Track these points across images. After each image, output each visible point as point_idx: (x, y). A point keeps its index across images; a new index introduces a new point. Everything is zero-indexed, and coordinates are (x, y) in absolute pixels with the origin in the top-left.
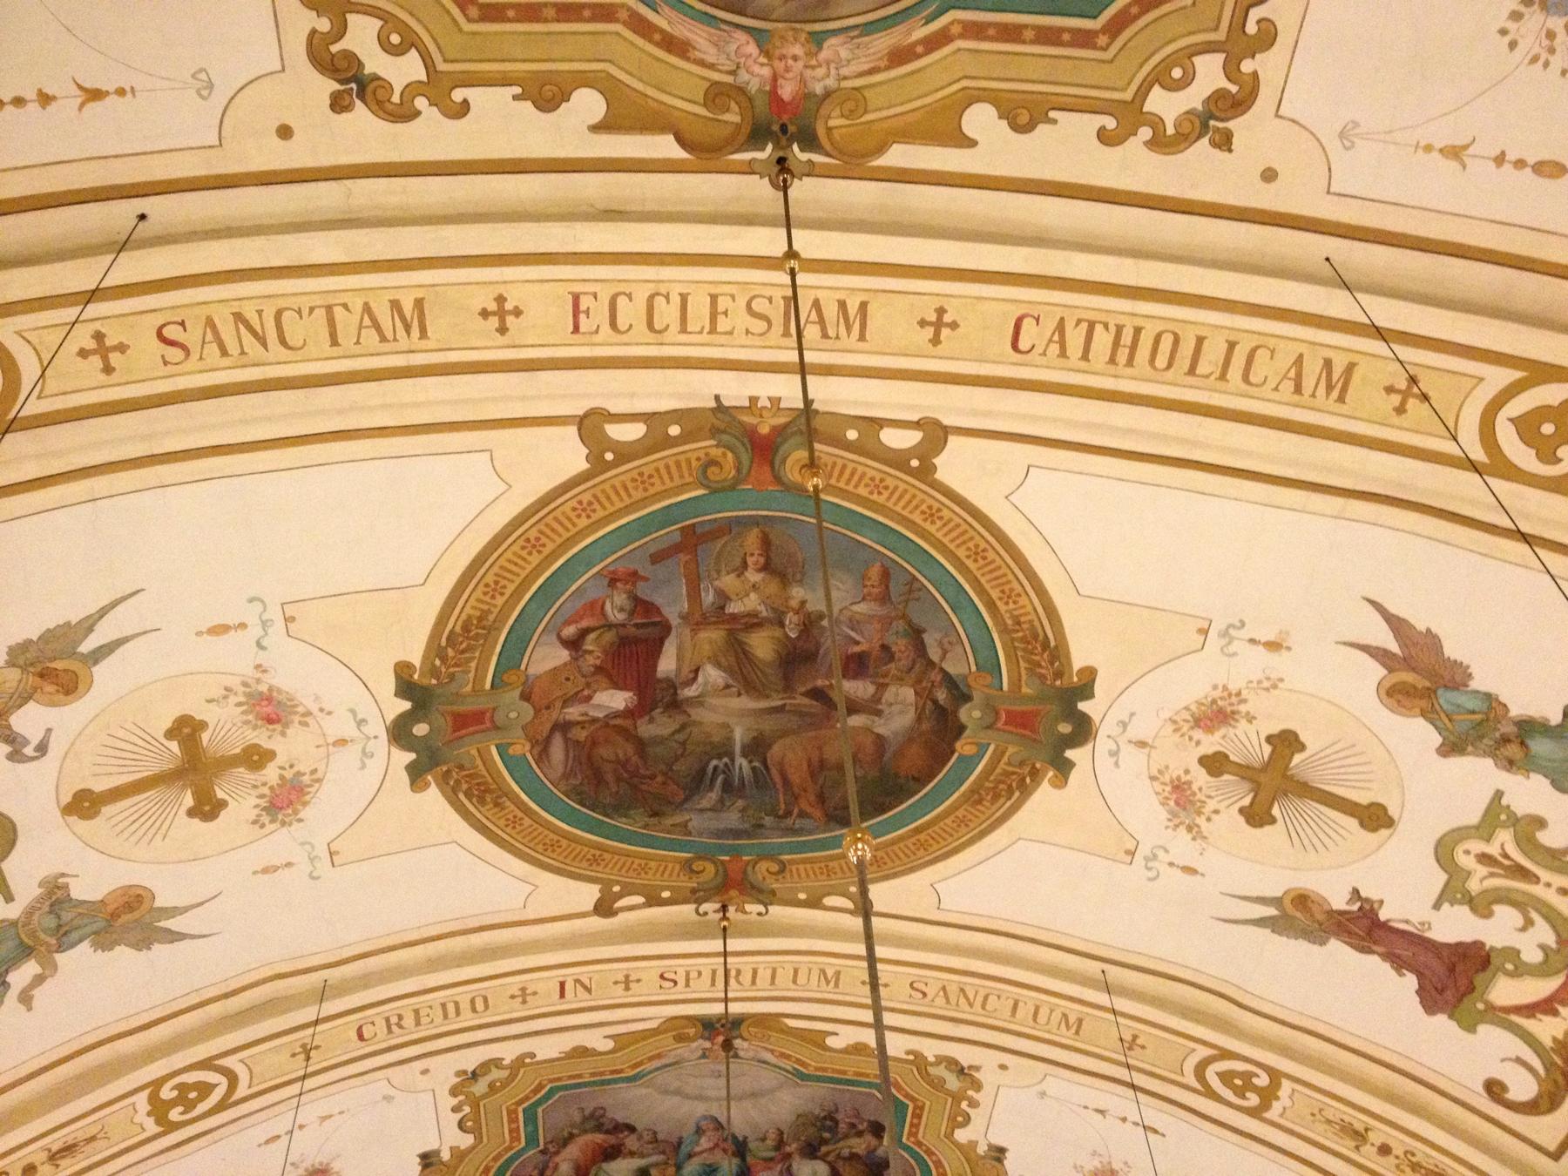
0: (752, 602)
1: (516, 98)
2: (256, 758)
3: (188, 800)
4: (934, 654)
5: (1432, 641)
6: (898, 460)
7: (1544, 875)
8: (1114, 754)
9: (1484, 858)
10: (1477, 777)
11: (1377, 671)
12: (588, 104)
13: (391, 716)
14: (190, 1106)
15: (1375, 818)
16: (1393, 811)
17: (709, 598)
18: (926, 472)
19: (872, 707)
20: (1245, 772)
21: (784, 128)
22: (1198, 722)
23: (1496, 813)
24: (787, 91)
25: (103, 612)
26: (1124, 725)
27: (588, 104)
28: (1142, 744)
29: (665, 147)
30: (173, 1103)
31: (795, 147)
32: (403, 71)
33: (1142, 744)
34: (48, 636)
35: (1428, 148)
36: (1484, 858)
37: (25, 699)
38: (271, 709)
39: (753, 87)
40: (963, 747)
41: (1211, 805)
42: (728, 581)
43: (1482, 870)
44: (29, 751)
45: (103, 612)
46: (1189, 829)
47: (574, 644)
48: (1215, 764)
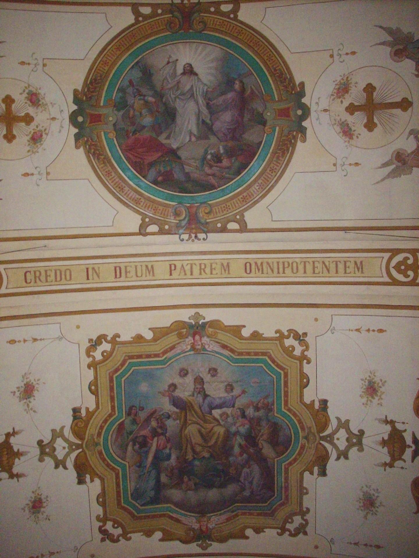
1: (263, 334)
6: (153, 222)
21: (197, 328)
24: (204, 529)
27: (158, 535)
31: (194, 323)
32: (289, 342)
35: (41, 340)
39: (196, 528)
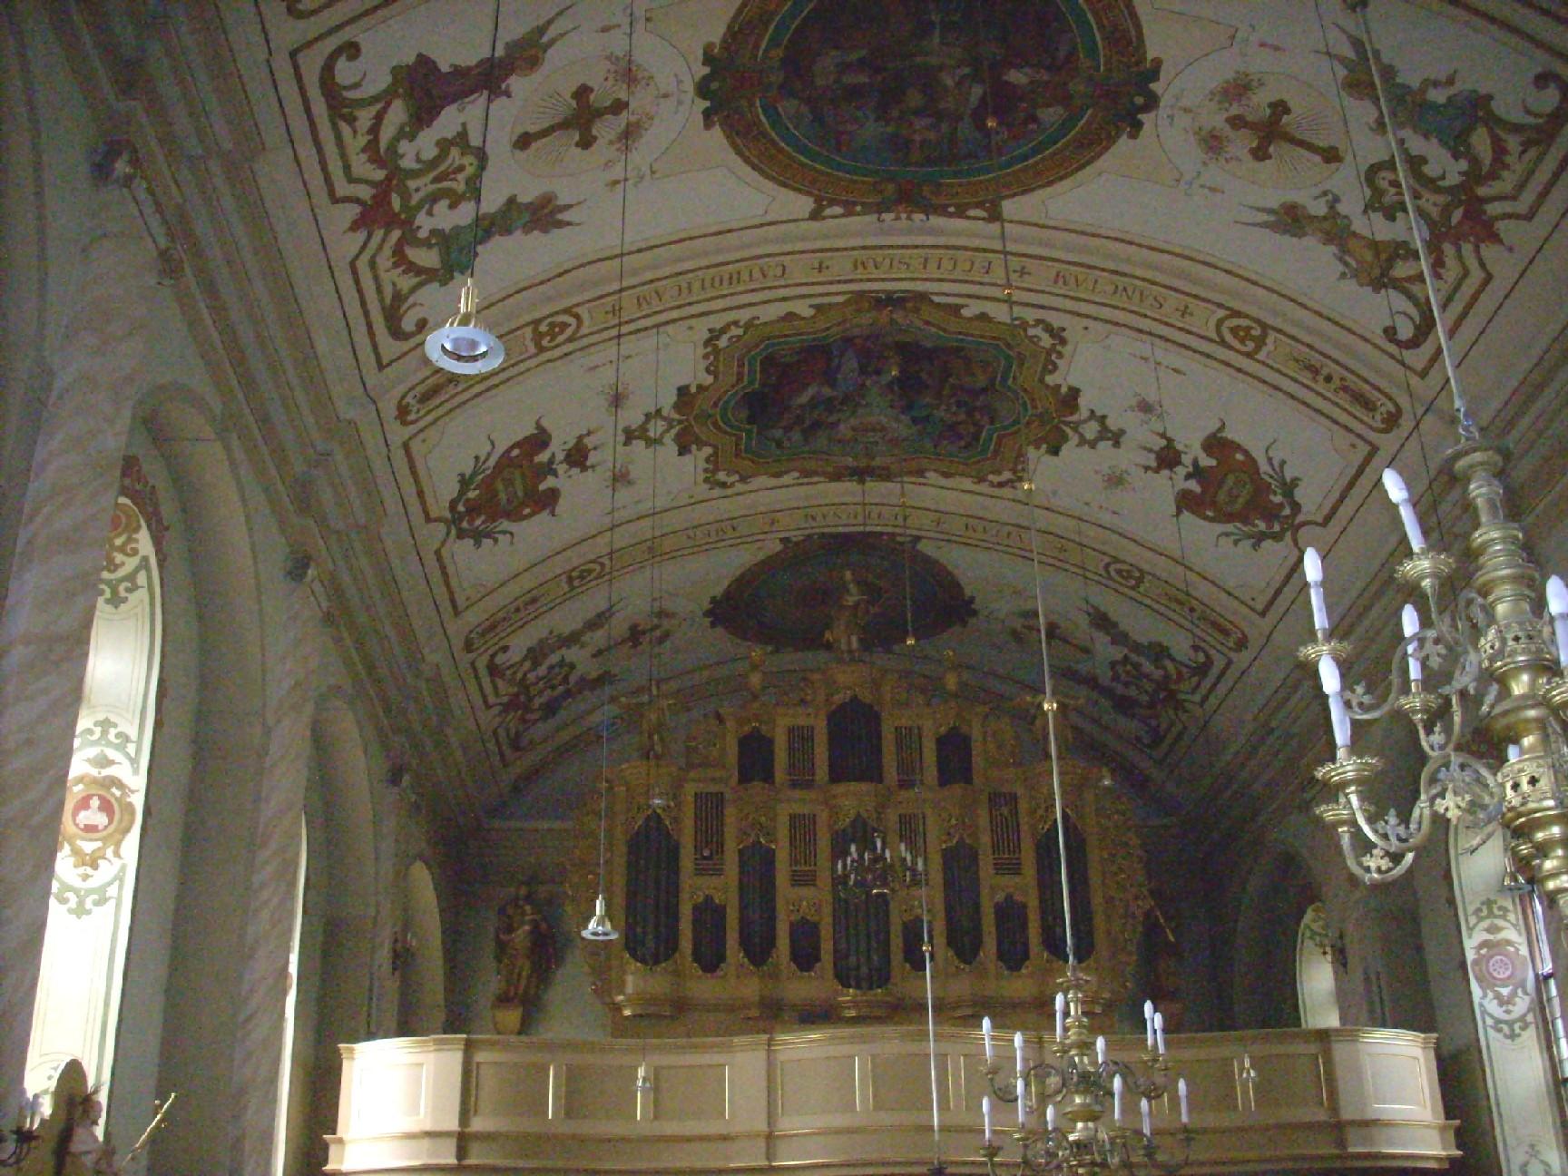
0: (920, 123)
2: (1237, 122)
3: (1285, 119)
4: (805, 109)
5: (545, 231)
7: (432, 187)
8: (680, 82)
9: (461, 169)
10: (492, 202)
11: (561, 201)
12: (965, 312)
13: (1152, 115)
14: (1248, 329)
15: (524, 141)
16: (518, 152)
17: (945, 127)
18: (818, 200)
19: (846, 67)
20: (599, 113)
22: (638, 125)
23: (474, 192)
25: (1254, 225)
26: (680, 103)
28: (666, 96)
29: (936, 299)
30: (1253, 339)
33: (666, 96)
34: (1285, 232)
36: (461, 169)
37: (1313, 218)
38: (1212, 143)
40: (778, 53)
41: (611, 82)
42: (932, 135)
43: (457, 163)
44: (1330, 197)
45: (1254, 225)
46: (617, 58)
47: (1033, 119)
48: (619, 107)
